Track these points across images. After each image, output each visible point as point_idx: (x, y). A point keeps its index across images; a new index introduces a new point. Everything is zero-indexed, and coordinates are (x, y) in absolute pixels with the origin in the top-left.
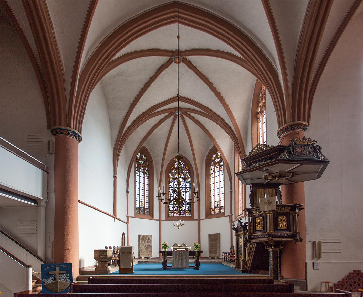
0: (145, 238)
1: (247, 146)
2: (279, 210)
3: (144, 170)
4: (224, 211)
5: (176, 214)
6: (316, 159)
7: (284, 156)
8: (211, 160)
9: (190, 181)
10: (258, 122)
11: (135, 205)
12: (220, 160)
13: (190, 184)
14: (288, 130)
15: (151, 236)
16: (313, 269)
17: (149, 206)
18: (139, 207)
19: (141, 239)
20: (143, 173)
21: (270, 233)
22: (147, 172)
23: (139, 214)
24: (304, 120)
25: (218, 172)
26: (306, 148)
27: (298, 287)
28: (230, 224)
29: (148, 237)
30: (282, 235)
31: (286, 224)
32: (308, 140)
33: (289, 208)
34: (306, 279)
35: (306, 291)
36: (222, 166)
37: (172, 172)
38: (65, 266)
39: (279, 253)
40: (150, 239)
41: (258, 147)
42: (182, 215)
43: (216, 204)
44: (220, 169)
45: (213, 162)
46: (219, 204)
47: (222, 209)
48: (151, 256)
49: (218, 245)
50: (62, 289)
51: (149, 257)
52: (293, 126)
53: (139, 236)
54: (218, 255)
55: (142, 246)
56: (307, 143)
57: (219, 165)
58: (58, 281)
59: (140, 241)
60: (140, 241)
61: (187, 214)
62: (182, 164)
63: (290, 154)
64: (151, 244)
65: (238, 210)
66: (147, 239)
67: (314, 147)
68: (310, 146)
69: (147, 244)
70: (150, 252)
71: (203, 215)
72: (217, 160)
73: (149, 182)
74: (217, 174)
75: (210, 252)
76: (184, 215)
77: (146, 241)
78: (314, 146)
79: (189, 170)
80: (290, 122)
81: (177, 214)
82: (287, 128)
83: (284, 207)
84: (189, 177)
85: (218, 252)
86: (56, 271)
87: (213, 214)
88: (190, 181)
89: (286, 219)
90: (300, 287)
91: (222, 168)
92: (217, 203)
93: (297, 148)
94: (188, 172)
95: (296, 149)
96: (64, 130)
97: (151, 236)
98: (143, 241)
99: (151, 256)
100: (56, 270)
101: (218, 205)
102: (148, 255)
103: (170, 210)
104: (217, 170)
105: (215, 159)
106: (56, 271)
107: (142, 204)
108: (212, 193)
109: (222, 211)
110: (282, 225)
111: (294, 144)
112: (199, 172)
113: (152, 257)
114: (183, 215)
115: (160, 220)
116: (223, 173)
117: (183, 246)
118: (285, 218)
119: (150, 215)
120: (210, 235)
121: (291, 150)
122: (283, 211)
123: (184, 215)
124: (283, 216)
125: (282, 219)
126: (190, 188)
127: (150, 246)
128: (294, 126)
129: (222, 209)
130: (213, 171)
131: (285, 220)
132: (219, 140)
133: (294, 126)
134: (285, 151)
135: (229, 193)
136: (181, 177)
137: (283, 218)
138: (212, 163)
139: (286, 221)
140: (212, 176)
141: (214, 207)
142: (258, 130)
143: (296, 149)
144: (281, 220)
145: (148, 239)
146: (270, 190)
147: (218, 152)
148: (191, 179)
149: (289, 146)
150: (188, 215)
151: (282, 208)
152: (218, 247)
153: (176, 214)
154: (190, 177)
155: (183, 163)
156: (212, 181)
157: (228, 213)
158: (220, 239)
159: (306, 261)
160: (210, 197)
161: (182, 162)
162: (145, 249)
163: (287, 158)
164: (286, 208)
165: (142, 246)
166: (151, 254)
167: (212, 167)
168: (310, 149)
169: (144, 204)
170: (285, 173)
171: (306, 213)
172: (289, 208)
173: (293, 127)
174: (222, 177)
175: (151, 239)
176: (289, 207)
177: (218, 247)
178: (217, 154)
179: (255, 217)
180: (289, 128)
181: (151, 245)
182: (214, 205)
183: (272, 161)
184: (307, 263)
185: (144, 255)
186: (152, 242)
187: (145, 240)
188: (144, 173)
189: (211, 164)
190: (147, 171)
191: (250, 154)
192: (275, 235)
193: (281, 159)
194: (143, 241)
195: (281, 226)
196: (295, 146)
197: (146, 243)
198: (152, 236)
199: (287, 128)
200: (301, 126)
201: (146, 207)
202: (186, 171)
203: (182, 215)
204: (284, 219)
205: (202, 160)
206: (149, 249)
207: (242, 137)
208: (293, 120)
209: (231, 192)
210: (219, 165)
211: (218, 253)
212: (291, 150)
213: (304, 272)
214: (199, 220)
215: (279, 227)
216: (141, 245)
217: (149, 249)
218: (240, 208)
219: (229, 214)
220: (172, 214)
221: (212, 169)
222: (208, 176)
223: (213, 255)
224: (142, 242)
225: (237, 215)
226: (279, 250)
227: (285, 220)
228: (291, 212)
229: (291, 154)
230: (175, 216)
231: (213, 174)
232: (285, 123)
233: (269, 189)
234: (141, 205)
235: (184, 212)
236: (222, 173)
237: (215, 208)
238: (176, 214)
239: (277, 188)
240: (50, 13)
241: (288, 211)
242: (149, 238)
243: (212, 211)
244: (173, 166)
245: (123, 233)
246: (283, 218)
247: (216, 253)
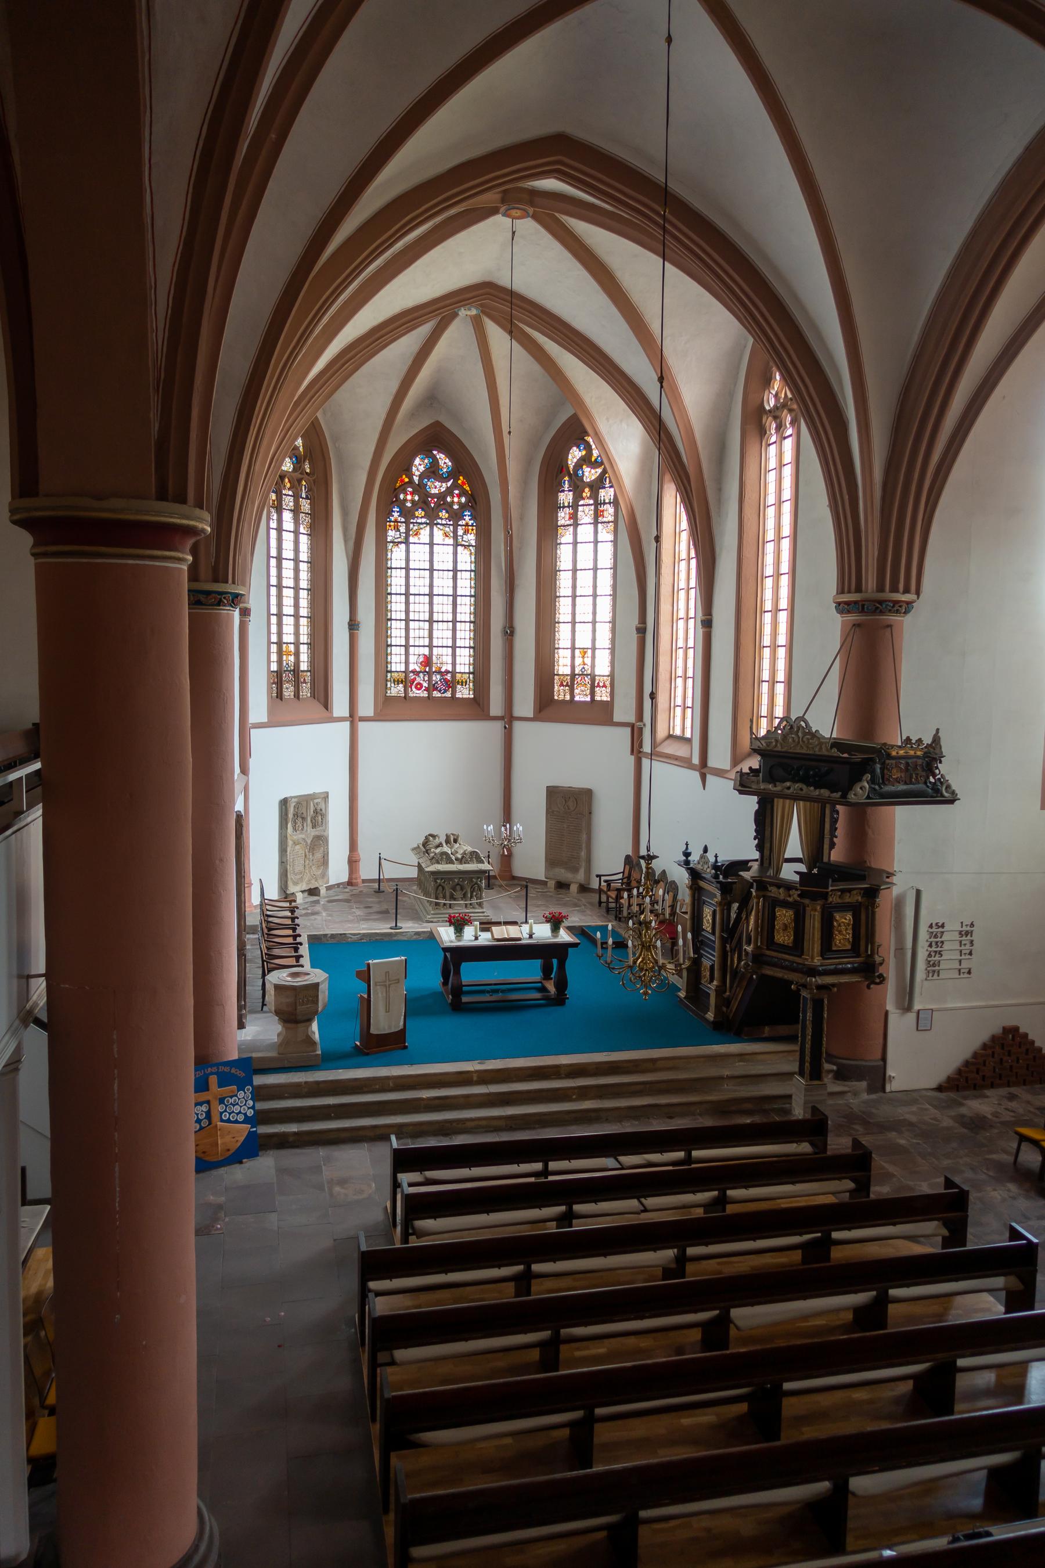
0: (304, 811)
1: (719, 508)
3: (296, 497)
4: (612, 694)
5: (414, 689)
8: (563, 468)
9: (474, 544)
10: (763, 444)
11: (269, 662)
12: (601, 479)
14: (865, 612)
15: (325, 796)
16: (917, 1030)
17: (312, 661)
18: (277, 672)
19: (290, 816)
20: (291, 510)
22: (305, 505)
23: (278, 700)
24: (907, 590)
25: (591, 528)
27: (864, 1084)
28: (632, 758)
30: (841, 966)
34: (884, 1059)
36: (605, 503)
37: (402, 496)
38: (233, 1071)
40: (321, 810)
42: (439, 695)
43: (578, 661)
44: (597, 514)
45: (570, 475)
46: (588, 661)
47: (601, 684)
48: (325, 880)
49: (584, 836)
50: (228, 1150)
51: (317, 888)
52: (878, 605)
53: (284, 803)
54: (580, 877)
55: (295, 843)
57: (595, 495)
58: (216, 1126)
60: (290, 825)
61: (459, 687)
62: (441, 463)
65: (668, 713)
66: (312, 812)
69: (311, 832)
71: (525, 703)
72: (590, 474)
73: (313, 548)
74: (585, 532)
75: (551, 862)
76: (448, 694)
79: (472, 495)
80: (873, 592)
81: (419, 686)
82: (863, 606)
84: (471, 522)
85: (583, 864)
86: (208, 1090)
87: (564, 701)
88: (474, 544)
90: (869, 1086)
91: (605, 514)
92: (583, 657)
93: (892, 768)
94: (468, 501)
96: (208, 593)
97: (325, 796)
98: (299, 821)
100: (210, 1088)
101: (584, 664)
102: (313, 881)
103: (391, 672)
104: (586, 514)
105: (579, 465)
106: (208, 1090)
107: (288, 654)
108: (561, 612)
109: (603, 695)
112: (514, 513)
114: (445, 691)
115: (353, 718)
116: (611, 537)
117: (471, 861)
119: (318, 700)
120: (553, 793)
123: (448, 694)
126: (473, 574)
127: (320, 842)
128: (881, 605)
129: (601, 684)
130: (570, 518)
131: (848, 925)
132: (608, 419)
133: (881, 605)
134: (864, 778)
135: (634, 636)
136: (439, 521)
138: (567, 478)
140: (566, 537)
141: (567, 671)
142: (762, 472)
145: (316, 811)
147: (590, 439)
148: (476, 535)
150: (464, 692)
152: (584, 845)
153: (414, 689)
154: (472, 525)
155: (447, 461)
156: (564, 554)
157: (625, 711)
158: (590, 813)
161: (442, 456)
162: (305, 856)
165: (295, 843)
166: (324, 875)
167: (566, 497)
169: (297, 654)
171: (895, 865)
172: (860, 894)
173: (878, 608)
174: (606, 552)
177: (584, 845)
178: (588, 448)
180: (867, 608)
181: (325, 834)
182: (568, 662)
185: (302, 881)
186: (327, 823)
187: (304, 819)
188: (296, 511)
189: (560, 484)
190: (307, 498)
192: (824, 968)
194: (299, 821)
197: (309, 830)
198: (327, 793)
199: (863, 606)
200: (900, 606)
201: (304, 666)
202: (459, 496)
203: (440, 691)
205: (529, 462)
206: (319, 855)
207: (706, 476)
208: (881, 588)
209: (642, 631)
210: (595, 495)
211: (582, 872)
213: (881, 1040)
214: (509, 718)
215: (833, 945)
216: (290, 843)
217: (319, 855)
218: (675, 706)
219: (632, 719)
220: (401, 685)
221: (564, 507)
222: (548, 532)
223: (564, 874)
224: (295, 829)
225: (661, 733)
230: (411, 695)
231: (571, 529)
232: (859, 590)
234: (284, 658)
235: (446, 681)
236: (606, 534)
237: (573, 675)
238: (416, 688)
240: (361, 494)
243: (562, 685)
244: (408, 471)
247: (575, 870)
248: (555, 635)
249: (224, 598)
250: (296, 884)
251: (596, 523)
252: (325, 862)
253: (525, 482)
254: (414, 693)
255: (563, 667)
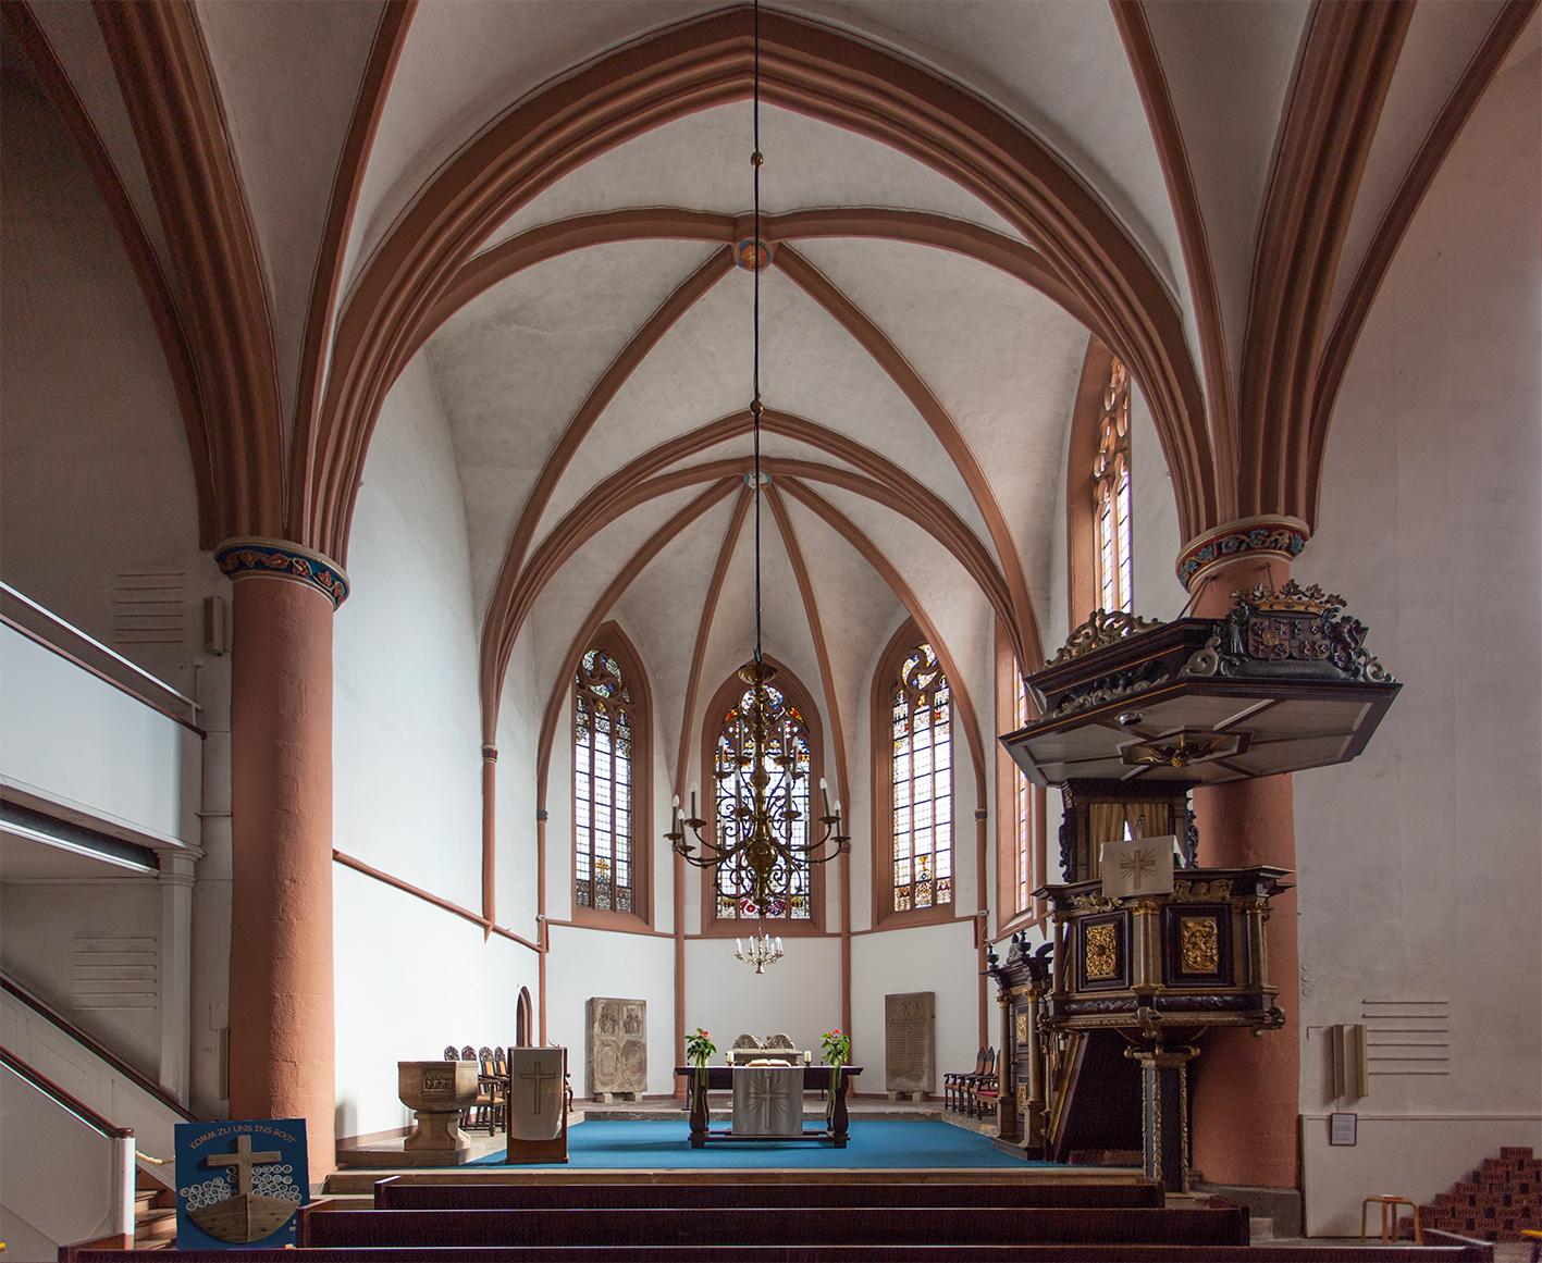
0: (615, 1014)
1: (1048, 619)
2: (1183, 892)
4: (953, 897)
5: (746, 912)
6: (1343, 675)
7: (1206, 662)
8: (896, 681)
9: (807, 770)
10: (1096, 519)
11: (574, 870)
13: (807, 783)
14: (1225, 555)
15: (643, 1004)
16: (1331, 1144)
17: (632, 878)
18: (589, 882)
19: (598, 1016)
20: (606, 734)
21: (1145, 992)
23: (590, 909)
24: (1291, 510)
25: (928, 733)
26: (1299, 630)
27: (1267, 1221)
28: (977, 951)
29: (630, 1007)
30: (1199, 998)
31: (1215, 951)
32: (1308, 594)
33: (1227, 886)
34: (1300, 1186)
35: (1299, 1236)
36: (942, 705)
38: (277, 1133)
39: (1184, 1074)
40: (637, 1017)
41: (1098, 623)
42: (772, 916)
43: (919, 868)
44: (933, 718)
45: (904, 687)
46: (928, 866)
47: (943, 887)
48: (642, 1087)
49: (927, 1042)
50: (264, 1230)
51: (631, 1093)
52: (1243, 537)
53: (591, 1003)
54: (924, 1084)
55: (604, 1044)
56: (1302, 608)
57: (930, 701)
58: (245, 1196)
59: (593, 1023)
60: (596, 1025)
61: (794, 908)
62: (772, 696)
63: (1230, 654)
64: (641, 1038)
65: (1012, 891)
66: (625, 1017)
67: (1335, 627)
68: (1317, 623)
69: (623, 1037)
70: (638, 1071)
71: (862, 916)
72: (924, 681)
73: (632, 773)
74: (922, 739)
75: (893, 1072)
76: (783, 916)
77: (621, 1023)
78: (1334, 621)
79: (804, 724)
80: (1233, 519)
82: (1219, 546)
83: (1208, 881)
84: (804, 751)
85: (926, 1070)
86: (237, 1152)
87: (905, 911)
88: (807, 770)
89: (1215, 932)
90: (1275, 1222)
91: (942, 715)
92: (924, 863)
93: (1263, 630)
94: (800, 731)
95: (1257, 634)
96: (271, 552)
97: (643, 1004)
98: (609, 1024)
99: (642, 1087)
100: (240, 1150)
101: (925, 870)
102: (627, 1086)
103: (723, 894)
104: (922, 721)
105: (913, 675)
106: (237, 1152)
107: (604, 867)
108: (899, 823)
109: (944, 898)
110: (1199, 959)
111: (1251, 613)
112: (846, 732)
113: (644, 1094)
114: (779, 913)
115: (679, 936)
116: (947, 737)
117: (778, 1045)
118: (1211, 927)
119: (639, 916)
120: (891, 1001)
121: (1236, 638)
122: (1203, 898)
123: (783, 916)
124: (1200, 919)
125: (1198, 931)
126: (807, 799)
127: (635, 1048)
128: (1249, 537)
129: (943, 887)
130: (906, 729)
131: (1210, 935)
133: (1249, 537)
134: (1210, 642)
135: (974, 823)
136: (771, 751)
137: (1204, 926)
138: (902, 692)
139: (1214, 938)
140: (902, 748)
141: (907, 880)
142: (1095, 551)
143: (1257, 634)
144: (1193, 935)
145: (630, 1016)
146: (1146, 807)
147: (926, 648)
148: (809, 761)
149: (1227, 620)
150: (799, 914)
151: (1196, 886)
152: (927, 1050)
153: (746, 912)
154: (806, 753)
155: (778, 693)
156: (901, 768)
157: (966, 905)
158: (933, 1017)
159: (1300, 1108)
160: (893, 839)
161: (773, 690)
162: (617, 1058)
163: (1221, 674)
164: (1216, 883)
165: (604, 1044)
166: (641, 1082)
167: (901, 710)
168: (1319, 636)
169: (613, 869)
170: (1213, 736)
171: (1299, 905)
172: (1227, 886)
173: (1243, 541)
174: (943, 753)
175: (644, 1015)
176: (1229, 879)
177: (927, 1050)
178: (923, 655)
179: (1082, 921)
181: (642, 1041)
182: (908, 871)
183: (1155, 684)
184: (1305, 1119)
185: (612, 1083)
186: (644, 1031)
187: (615, 1022)
188: (613, 736)
189: (895, 698)
190: (626, 725)
191: (1062, 656)
192: (1170, 999)
193: (1193, 675)
194: (609, 1024)
195: (1195, 962)
196: (1253, 620)
197: (621, 1035)
198: (645, 1002)
199: (1219, 546)
200: (1280, 535)
201: (622, 881)
202: (791, 726)
203: (773, 913)
204: (1207, 929)
206: (634, 1061)
207: (1029, 584)
208: (1246, 509)
209: (982, 815)
210: (930, 701)
211: (925, 1078)
212: (1236, 638)
213: (1293, 1159)
214: (846, 935)
215: (1184, 966)
216: (597, 1042)
217: (634, 1061)
218: (1020, 884)
219: (974, 911)
220: (732, 908)
221: (900, 720)
222: (883, 748)
223: (905, 1084)
224: (603, 1029)
225: (1006, 912)
226: (1184, 1064)
227: (1210, 935)
228: (1237, 902)
229: (1238, 655)
230: (742, 917)
231: (907, 739)
232: (1211, 523)
233: (1141, 803)
234: (597, 870)
235: (780, 903)
236: (942, 735)
237: (914, 883)
238: (748, 909)
239: (1177, 801)
240: (213, 56)
241: (1224, 898)
242: (633, 1014)
243: (902, 895)
244: (737, 706)
245: (524, 990)
246: (1204, 926)
247: (919, 1078)
248: (893, 848)
249: (297, 562)
250: (604, 1084)
251: (932, 726)
252: (642, 1068)
253: (856, 700)
254: (746, 915)
255: (903, 879)
